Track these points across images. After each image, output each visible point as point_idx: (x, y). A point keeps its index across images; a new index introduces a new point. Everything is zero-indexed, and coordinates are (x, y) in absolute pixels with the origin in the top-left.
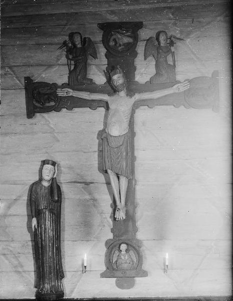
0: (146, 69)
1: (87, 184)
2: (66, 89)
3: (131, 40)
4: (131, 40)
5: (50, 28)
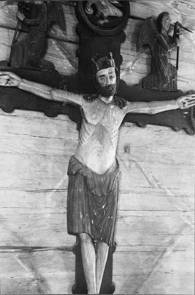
0: (134, 62)
1: (30, 250)
2: (8, 73)
3: (119, 13)
4: (119, 13)
5: (181, 144)
